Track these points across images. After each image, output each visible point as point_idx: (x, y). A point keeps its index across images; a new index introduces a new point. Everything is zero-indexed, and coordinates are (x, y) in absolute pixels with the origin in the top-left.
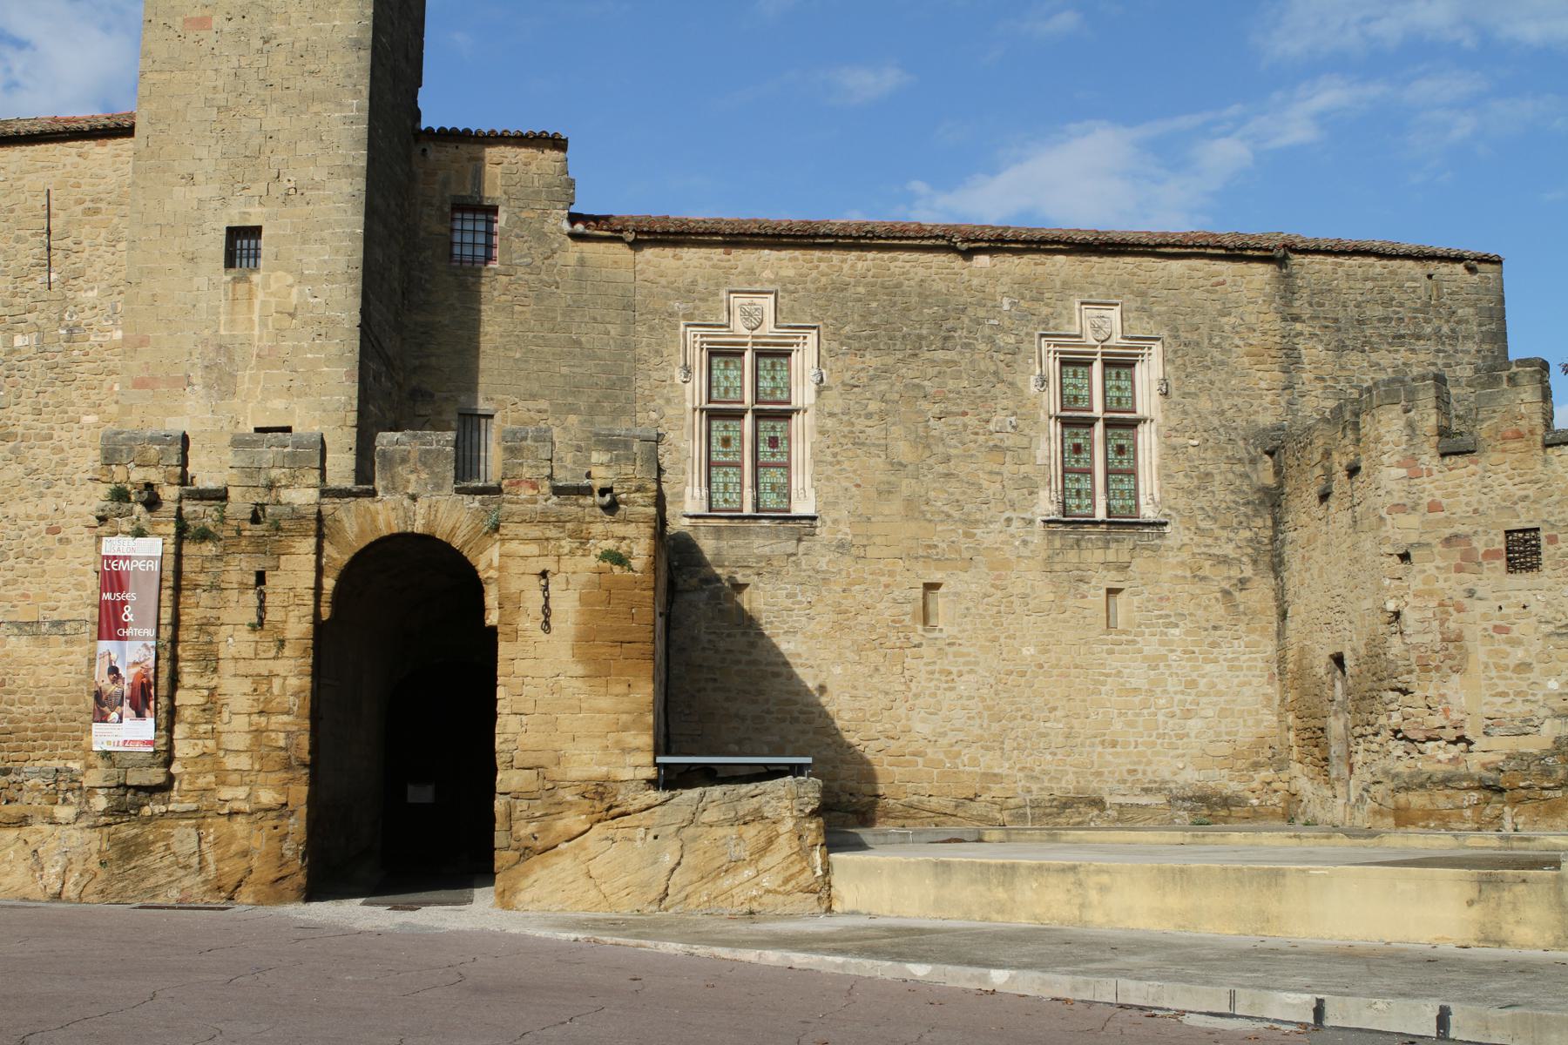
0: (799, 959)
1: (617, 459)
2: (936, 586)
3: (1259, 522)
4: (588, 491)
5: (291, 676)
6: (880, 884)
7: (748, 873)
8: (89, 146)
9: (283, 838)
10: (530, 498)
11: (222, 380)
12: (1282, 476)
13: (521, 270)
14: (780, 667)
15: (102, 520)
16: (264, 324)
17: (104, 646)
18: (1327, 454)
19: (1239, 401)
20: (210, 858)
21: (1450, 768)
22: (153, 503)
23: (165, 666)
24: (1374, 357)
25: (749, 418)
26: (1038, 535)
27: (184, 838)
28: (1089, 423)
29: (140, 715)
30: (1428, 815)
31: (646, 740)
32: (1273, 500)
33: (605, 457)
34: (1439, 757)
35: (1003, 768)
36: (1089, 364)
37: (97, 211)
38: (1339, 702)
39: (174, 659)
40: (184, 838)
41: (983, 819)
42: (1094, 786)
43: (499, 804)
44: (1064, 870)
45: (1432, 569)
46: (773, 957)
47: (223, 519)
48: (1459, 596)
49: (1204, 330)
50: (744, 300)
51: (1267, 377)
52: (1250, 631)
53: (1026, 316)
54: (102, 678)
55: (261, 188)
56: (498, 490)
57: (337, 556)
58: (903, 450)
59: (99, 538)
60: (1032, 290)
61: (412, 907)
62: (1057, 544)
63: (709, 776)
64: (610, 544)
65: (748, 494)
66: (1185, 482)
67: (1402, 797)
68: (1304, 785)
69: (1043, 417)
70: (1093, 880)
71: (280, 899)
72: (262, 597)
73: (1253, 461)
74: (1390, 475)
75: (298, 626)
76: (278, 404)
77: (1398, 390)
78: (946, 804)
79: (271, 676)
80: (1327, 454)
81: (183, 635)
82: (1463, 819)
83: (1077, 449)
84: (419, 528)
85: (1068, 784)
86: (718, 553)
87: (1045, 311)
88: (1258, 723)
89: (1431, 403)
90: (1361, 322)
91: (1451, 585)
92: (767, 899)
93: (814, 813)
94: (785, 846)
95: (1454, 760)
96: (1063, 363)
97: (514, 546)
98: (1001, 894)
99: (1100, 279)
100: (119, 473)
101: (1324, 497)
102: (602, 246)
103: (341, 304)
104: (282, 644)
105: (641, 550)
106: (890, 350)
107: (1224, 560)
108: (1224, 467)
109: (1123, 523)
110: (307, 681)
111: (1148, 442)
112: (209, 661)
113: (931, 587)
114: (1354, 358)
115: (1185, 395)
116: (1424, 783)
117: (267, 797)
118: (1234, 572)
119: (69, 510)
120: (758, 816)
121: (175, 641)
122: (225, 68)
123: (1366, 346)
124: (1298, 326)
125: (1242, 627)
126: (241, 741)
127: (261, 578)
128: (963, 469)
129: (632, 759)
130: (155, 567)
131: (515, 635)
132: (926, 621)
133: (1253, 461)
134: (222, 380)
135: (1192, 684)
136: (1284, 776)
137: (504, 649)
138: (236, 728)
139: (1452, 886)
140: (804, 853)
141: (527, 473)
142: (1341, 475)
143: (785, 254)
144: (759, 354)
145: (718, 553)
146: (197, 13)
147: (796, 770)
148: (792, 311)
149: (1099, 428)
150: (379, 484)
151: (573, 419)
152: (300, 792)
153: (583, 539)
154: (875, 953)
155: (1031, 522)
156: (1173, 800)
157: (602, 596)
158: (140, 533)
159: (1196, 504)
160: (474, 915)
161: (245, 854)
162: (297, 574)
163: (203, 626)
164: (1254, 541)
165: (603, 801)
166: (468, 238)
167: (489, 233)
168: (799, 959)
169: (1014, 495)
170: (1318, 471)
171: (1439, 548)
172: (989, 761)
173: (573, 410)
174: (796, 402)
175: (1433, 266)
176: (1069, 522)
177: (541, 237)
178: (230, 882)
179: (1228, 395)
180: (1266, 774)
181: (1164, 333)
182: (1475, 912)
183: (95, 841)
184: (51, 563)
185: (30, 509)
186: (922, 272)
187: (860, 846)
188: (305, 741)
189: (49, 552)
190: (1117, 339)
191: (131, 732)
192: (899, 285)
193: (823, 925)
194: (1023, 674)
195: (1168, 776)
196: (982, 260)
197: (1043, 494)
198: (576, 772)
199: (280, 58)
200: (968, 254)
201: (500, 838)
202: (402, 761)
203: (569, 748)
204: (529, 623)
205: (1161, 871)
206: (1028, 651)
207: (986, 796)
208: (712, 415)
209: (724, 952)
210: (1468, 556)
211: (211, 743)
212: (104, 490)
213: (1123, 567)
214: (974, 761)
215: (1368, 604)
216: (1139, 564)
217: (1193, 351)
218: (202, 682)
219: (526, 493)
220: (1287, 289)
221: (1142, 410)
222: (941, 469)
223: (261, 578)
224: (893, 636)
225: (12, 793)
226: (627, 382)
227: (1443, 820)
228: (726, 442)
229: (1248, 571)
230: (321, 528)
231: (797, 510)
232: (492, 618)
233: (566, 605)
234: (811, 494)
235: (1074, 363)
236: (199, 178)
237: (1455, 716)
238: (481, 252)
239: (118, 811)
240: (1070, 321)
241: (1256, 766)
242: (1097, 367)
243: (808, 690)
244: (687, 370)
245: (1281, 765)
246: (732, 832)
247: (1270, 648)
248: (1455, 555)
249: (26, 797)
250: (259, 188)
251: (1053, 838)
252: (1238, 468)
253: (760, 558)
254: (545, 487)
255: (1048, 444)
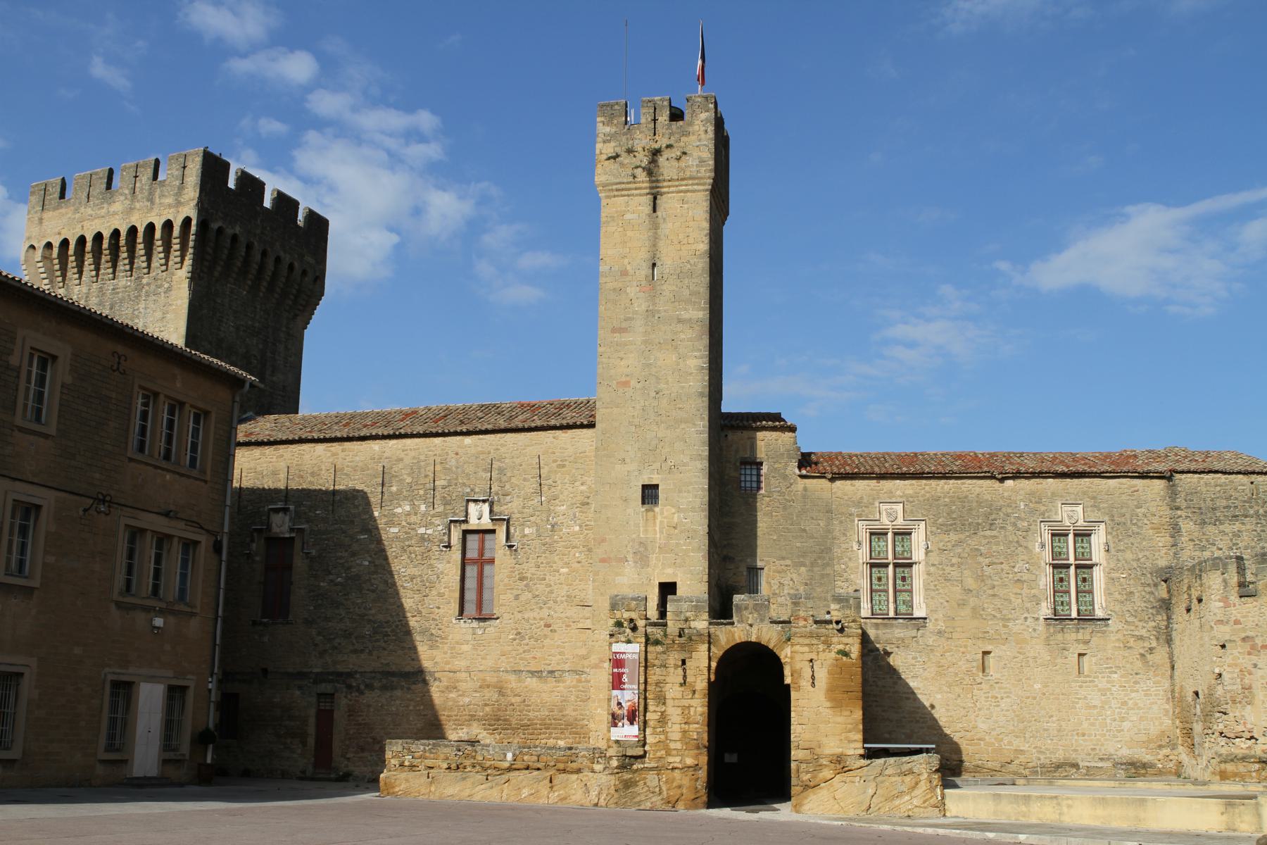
0: (941, 831)
1: (843, 607)
2: (989, 653)
3: (1160, 617)
4: (830, 622)
5: (699, 707)
6: (968, 803)
7: (907, 798)
8: (558, 433)
9: (697, 780)
10: (803, 626)
11: (642, 558)
12: (1169, 592)
13: (775, 495)
14: (911, 693)
15: (612, 635)
16: (661, 532)
17: (615, 692)
18: (1189, 588)
19: (1147, 553)
20: (664, 788)
21: (1247, 752)
22: (634, 629)
23: (642, 701)
24: (1221, 527)
25: (891, 567)
26: (1041, 626)
27: (652, 779)
28: (1068, 566)
29: (632, 724)
30: (1235, 775)
31: (860, 736)
32: (1166, 606)
33: (837, 607)
34: (1242, 746)
35: (1025, 747)
36: (1067, 535)
37: (564, 466)
38: (1198, 713)
39: (646, 699)
40: (652, 779)
41: (1015, 773)
42: (1073, 757)
43: (793, 765)
44: (1052, 798)
45: (1236, 653)
46: (930, 831)
47: (666, 635)
48: (1250, 667)
49: (1128, 516)
50: (888, 506)
51: (1163, 540)
52: (1156, 675)
53: (1033, 512)
54: (615, 708)
55: (657, 465)
56: (789, 622)
57: (718, 652)
58: (970, 583)
59: (611, 644)
60: (1036, 498)
61: (757, 811)
62: (1052, 630)
63: (887, 753)
64: (841, 647)
65: (892, 606)
66: (1119, 597)
67: (1223, 766)
68: (1184, 758)
69: (1043, 564)
70: (1065, 802)
71: (696, 807)
72: (684, 670)
73: (1156, 585)
74: (1214, 605)
75: (701, 684)
76: (670, 571)
77: (1218, 564)
78: (996, 765)
79: (689, 707)
80: (1189, 588)
81: (649, 688)
82: (1252, 778)
83: (1061, 580)
84: (753, 639)
85: (1059, 756)
86: (877, 637)
87: (1043, 508)
88: (1161, 724)
89: (1235, 570)
90: (1214, 509)
91: (1246, 662)
92: (916, 810)
93: (937, 771)
94: (923, 786)
95: (1249, 748)
96: (1053, 535)
97: (797, 648)
98: (1024, 808)
99: (1071, 491)
100: (618, 614)
101: (1188, 610)
102: (815, 481)
103: (698, 522)
104: (694, 692)
105: (855, 650)
106: (962, 531)
107: (1141, 638)
108: (1140, 588)
109: (1087, 619)
110: (706, 709)
111: (1098, 575)
112: (662, 700)
113: (986, 653)
114: (1210, 529)
115: (1118, 551)
116: (1233, 759)
117: (689, 761)
118: (1147, 644)
119: (555, 615)
120: (911, 772)
121: (645, 690)
122: (638, 407)
123: (1217, 522)
124: (1179, 512)
125: (1151, 673)
126: (677, 736)
127: (684, 662)
128: (1001, 592)
129: (853, 745)
130: (636, 657)
131: (798, 689)
132: (984, 671)
133: (1156, 585)
134: (642, 558)
135: (1125, 703)
136: (1175, 752)
137: (793, 695)
138: (674, 730)
139: (1215, 806)
140: (933, 789)
141: (802, 614)
142: (1195, 601)
143: (907, 482)
144: (895, 534)
145: (877, 637)
146: (624, 379)
147: (928, 751)
148: (912, 512)
149: (1072, 569)
150: (735, 619)
151: (803, 569)
152: (704, 759)
153: (828, 644)
154: (971, 829)
155: (1037, 619)
156: (1115, 765)
157: (838, 671)
158: (629, 642)
159: (1125, 609)
160: (783, 813)
161: (680, 787)
162: (701, 664)
163: (657, 684)
164: (1157, 628)
165: (840, 765)
166: (748, 478)
167: (759, 475)
168: (941, 831)
169: (1029, 605)
170: (1186, 596)
171: (1239, 643)
172: (1017, 743)
173: (803, 564)
174: (915, 559)
175: (1253, 477)
176: (1058, 618)
177: (785, 477)
178: (674, 799)
179: (1141, 550)
180: (1166, 751)
181: (1106, 518)
182: (1224, 817)
183: (613, 780)
184: (547, 642)
185: (535, 615)
186: (978, 490)
187: (955, 786)
188: (705, 736)
189: (546, 636)
190: (1081, 522)
191: (628, 732)
192: (966, 497)
193: (942, 821)
194: (1035, 698)
195: (1112, 751)
196: (1009, 483)
197: (1044, 604)
198: (828, 751)
199: (664, 402)
200: (1002, 480)
201: (794, 781)
202: (748, 743)
203: (825, 740)
204: (805, 683)
205: (1094, 799)
206: (1037, 686)
207: (1016, 762)
208: (872, 566)
209: (909, 829)
210: (1253, 647)
211: (663, 737)
212: (612, 622)
213: (1087, 642)
214: (1010, 743)
215: (1207, 668)
216: (1095, 640)
217: (1121, 526)
218: (658, 709)
219: (802, 623)
220: (1173, 493)
221: (1095, 559)
222: (991, 592)
223: (684, 662)
224: (967, 678)
225: (573, 758)
226: (829, 550)
227: (1242, 778)
228: (879, 579)
229: (1154, 644)
230: (710, 640)
231: (917, 614)
232: (788, 680)
233: (822, 675)
234: (924, 606)
235: (1058, 535)
236: (628, 460)
237: (1249, 726)
238: (755, 485)
239: (622, 767)
240: (1056, 513)
241: (1160, 747)
242: (1071, 537)
243: (924, 706)
244: (860, 543)
245: (1174, 747)
246: (899, 779)
247: (1167, 684)
248: (1247, 646)
249: (580, 760)
250: (657, 465)
251: (1051, 784)
252: (1148, 589)
253: (898, 639)
254: (811, 620)
255: (1046, 579)
